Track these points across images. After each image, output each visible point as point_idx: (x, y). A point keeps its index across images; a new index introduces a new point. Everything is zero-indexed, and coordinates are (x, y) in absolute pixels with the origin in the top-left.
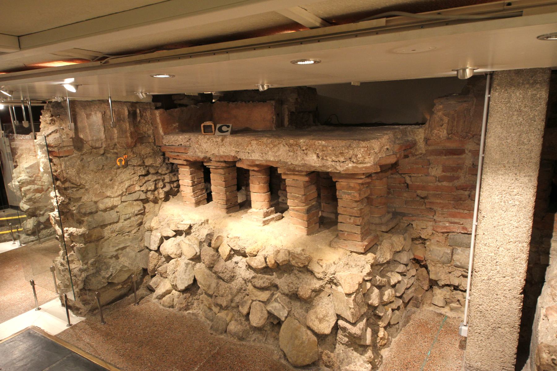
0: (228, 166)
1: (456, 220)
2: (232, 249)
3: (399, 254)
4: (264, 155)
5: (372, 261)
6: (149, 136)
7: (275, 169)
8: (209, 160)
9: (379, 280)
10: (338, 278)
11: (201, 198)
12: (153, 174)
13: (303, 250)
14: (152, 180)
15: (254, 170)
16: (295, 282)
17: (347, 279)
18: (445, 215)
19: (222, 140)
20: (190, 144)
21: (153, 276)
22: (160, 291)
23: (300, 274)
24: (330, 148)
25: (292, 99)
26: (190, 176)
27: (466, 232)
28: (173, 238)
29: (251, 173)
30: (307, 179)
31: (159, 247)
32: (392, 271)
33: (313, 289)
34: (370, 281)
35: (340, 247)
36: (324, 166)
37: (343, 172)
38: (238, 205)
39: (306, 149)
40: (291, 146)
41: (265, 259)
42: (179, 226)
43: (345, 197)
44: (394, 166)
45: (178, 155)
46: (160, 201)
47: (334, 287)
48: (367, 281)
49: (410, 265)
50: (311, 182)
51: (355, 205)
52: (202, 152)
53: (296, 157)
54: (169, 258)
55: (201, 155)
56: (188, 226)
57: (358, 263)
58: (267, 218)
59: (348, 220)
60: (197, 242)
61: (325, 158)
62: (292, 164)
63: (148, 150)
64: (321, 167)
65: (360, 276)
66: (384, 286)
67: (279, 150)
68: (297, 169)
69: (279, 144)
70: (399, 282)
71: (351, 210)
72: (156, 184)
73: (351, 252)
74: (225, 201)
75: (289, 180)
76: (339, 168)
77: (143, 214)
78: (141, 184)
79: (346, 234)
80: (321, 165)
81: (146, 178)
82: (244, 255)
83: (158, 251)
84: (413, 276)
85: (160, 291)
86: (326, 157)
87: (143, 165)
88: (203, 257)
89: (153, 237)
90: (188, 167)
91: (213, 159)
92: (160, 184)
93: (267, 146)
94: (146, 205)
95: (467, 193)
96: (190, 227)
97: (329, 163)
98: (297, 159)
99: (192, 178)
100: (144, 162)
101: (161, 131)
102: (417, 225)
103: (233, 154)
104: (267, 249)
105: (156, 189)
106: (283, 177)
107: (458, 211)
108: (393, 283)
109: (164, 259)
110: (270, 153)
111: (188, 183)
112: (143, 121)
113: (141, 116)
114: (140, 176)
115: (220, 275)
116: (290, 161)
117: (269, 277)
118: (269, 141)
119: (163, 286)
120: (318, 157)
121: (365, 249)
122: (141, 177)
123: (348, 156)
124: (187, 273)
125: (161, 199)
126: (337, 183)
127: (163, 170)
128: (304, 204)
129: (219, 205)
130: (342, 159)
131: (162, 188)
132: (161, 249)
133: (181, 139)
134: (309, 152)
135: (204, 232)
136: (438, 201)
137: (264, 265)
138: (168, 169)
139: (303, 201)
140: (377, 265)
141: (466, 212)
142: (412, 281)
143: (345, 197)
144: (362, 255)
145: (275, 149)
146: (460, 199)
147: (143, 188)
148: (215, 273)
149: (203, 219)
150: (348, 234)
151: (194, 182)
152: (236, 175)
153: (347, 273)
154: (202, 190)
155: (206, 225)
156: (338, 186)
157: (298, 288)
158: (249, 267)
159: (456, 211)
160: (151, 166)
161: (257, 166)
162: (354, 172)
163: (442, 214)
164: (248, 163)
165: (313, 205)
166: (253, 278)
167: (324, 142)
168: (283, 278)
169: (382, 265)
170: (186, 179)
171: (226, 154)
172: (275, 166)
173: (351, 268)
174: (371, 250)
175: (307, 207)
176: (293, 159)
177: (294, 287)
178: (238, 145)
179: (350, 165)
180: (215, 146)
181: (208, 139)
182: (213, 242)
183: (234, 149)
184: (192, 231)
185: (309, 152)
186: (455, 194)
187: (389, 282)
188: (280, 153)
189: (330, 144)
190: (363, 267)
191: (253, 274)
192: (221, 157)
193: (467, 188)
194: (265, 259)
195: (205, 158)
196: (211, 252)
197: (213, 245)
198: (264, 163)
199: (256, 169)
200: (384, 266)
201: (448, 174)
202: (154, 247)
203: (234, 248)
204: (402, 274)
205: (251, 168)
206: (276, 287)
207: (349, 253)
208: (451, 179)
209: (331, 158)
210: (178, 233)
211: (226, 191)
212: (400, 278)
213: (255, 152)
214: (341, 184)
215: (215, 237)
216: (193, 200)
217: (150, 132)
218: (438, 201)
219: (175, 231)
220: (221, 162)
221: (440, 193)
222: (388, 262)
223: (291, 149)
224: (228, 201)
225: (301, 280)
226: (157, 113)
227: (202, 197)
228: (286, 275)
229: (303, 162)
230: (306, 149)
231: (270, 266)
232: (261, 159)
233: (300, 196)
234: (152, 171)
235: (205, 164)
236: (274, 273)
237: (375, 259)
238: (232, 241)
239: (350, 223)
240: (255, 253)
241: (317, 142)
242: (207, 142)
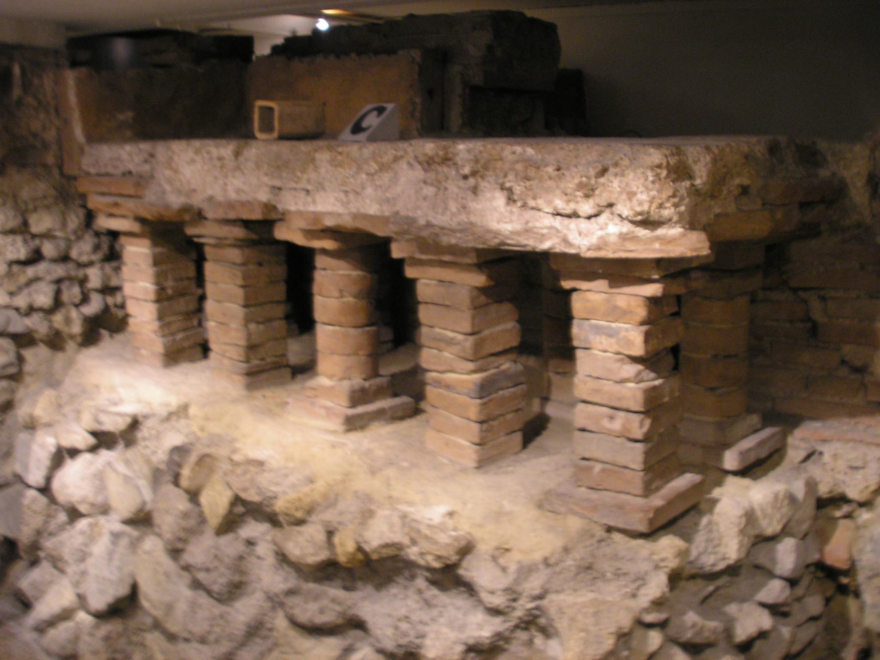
0: (254, 236)
2: (237, 500)
3: (770, 545)
4: (352, 196)
5: (673, 563)
6: (45, 146)
7: (384, 244)
8: (199, 216)
9: (694, 626)
10: (552, 611)
11: (183, 339)
12: (55, 261)
13: (451, 514)
14: (49, 278)
15: (324, 251)
16: (415, 617)
17: (580, 617)
21: (34, 563)
22: (44, 609)
25: (475, 46)
29: (320, 261)
30: (479, 280)
31: (49, 479)
32: (743, 600)
33: (471, 642)
34: (662, 625)
38: (278, 365)
39: (474, 173)
40: (428, 163)
41: (330, 534)
42: (103, 418)
44: (773, 255)
45: (116, 205)
46: (71, 346)
47: (539, 640)
48: (650, 626)
49: (805, 582)
50: (492, 294)
51: (631, 369)
52: (179, 192)
53: (445, 202)
54: (74, 514)
55: (176, 201)
56: (129, 420)
57: (626, 567)
58: (360, 410)
60: (146, 470)
61: (532, 203)
62: (429, 225)
63: (42, 187)
65: (628, 609)
66: (710, 645)
67: (395, 180)
68: (445, 240)
69: (396, 159)
70: (762, 635)
71: (618, 387)
72: (58, 293)
73: (610, 529)
74: (241, 351)
75: (427, 282)
77: (16, 377)
78: (13, 288)
81: (31, 271)
82: (273, 520)
83: (45, 490)
84: (813, 619)
85: (44, 609)
86: (534, 198)
87: (23, 229)
88: (157, 519)
89: (35, 448)
90: (146, 242)
91: (210, 214)
92: (72, 293)
93: (360, 169)
94: (28, 354)
97: (545, 221)
98: (446, 208)
100: (25, 224)
101: (78, 132)
102: (835, 456)
103: (263, 196)
104: (341, 506)
105: (58, 304)
106: (410, 272)
108: (742, 633)
109: (62, 517)
110: (369, 191)
112: (30, 100)
113: (26, 86)
114: (11, 263)
115: (201, 576)
116: (424, 214)
117: (340, 593)
119: (55, 597)
120: (511, 200)
121: (651, 521)
122: (15, 268)
124: (116, 563)
125: (72, 337)
126: (575, 297)
127: (83, 250)
128: (471, 366)
129: (226, 362)
130: (586, 208)
131: (77, 306)
132: (56, 485)
133: (128, 155)
134: (483, 184)
135: (158, 444)
137: (323, 555)
138: (97, 248)
139: (469, 353)
140: (693, 577)
142: (807, 633)
143: (599, 342)
144: (640, 542)
145: (385, 178)
147: (21, 301)
148: (187, 568)
149: (174, 401)
150: (603, 471)
152: (281, 271)
153: (586, 596)
155: (183, 422)
156: (577, 304)
157: (423, 636)
158: (283, 558)
160: (47, 235)
161: (334, 233)
162: (624, 255)
164: (303, 224)
165: (505, 375)
166: (291, 592)
167: (530, 151)
169: (712, 576)
170: (138, 279)
171: (244, 198)
172: (381, 234)
173: (600, 583)
174: (675, 527)
175: (477, 377)
176: (434, 207)
177: (412, 633)
178: (279, 166)
182: (186, 472)
184: (139, 435)
185: (483, 184)
187: (728, 633)
188: (399, 189)
189: (551, 158)
190: (641, 580)
191: (293, 581)
192: (231, 205)
194: (330, 534)
195: (186, 209)
196: (182, 504)
197: (184, 482)
198: (348, 222)
199: (329, 244)
200: (719, 582)
202: (36, 477)
203: (243, 495)
204: (776, 610)
205: (316, 244)
206: (358, 624)
207: (600, 533)
209: (549, 203)
210: (103, 440)
211: (248, 320)
212: (765, 621)
213: (336, 189)
214: (589, 298)
215: (193, 458)
216: (158, 345)
217: (50, 135)
219: (94, 434)
222: (733, 570)
223: (431, 175)
224: (252, 348)
226: (71, 77)
229: (463, 217)
230: (474, 173)
231: (342, 559)
233: (460, 337)
234: (48, 249)
237: (683, 554)
238: (239, 471)
239: (609, 433)
240: (299, 515)
242: (193, 161)
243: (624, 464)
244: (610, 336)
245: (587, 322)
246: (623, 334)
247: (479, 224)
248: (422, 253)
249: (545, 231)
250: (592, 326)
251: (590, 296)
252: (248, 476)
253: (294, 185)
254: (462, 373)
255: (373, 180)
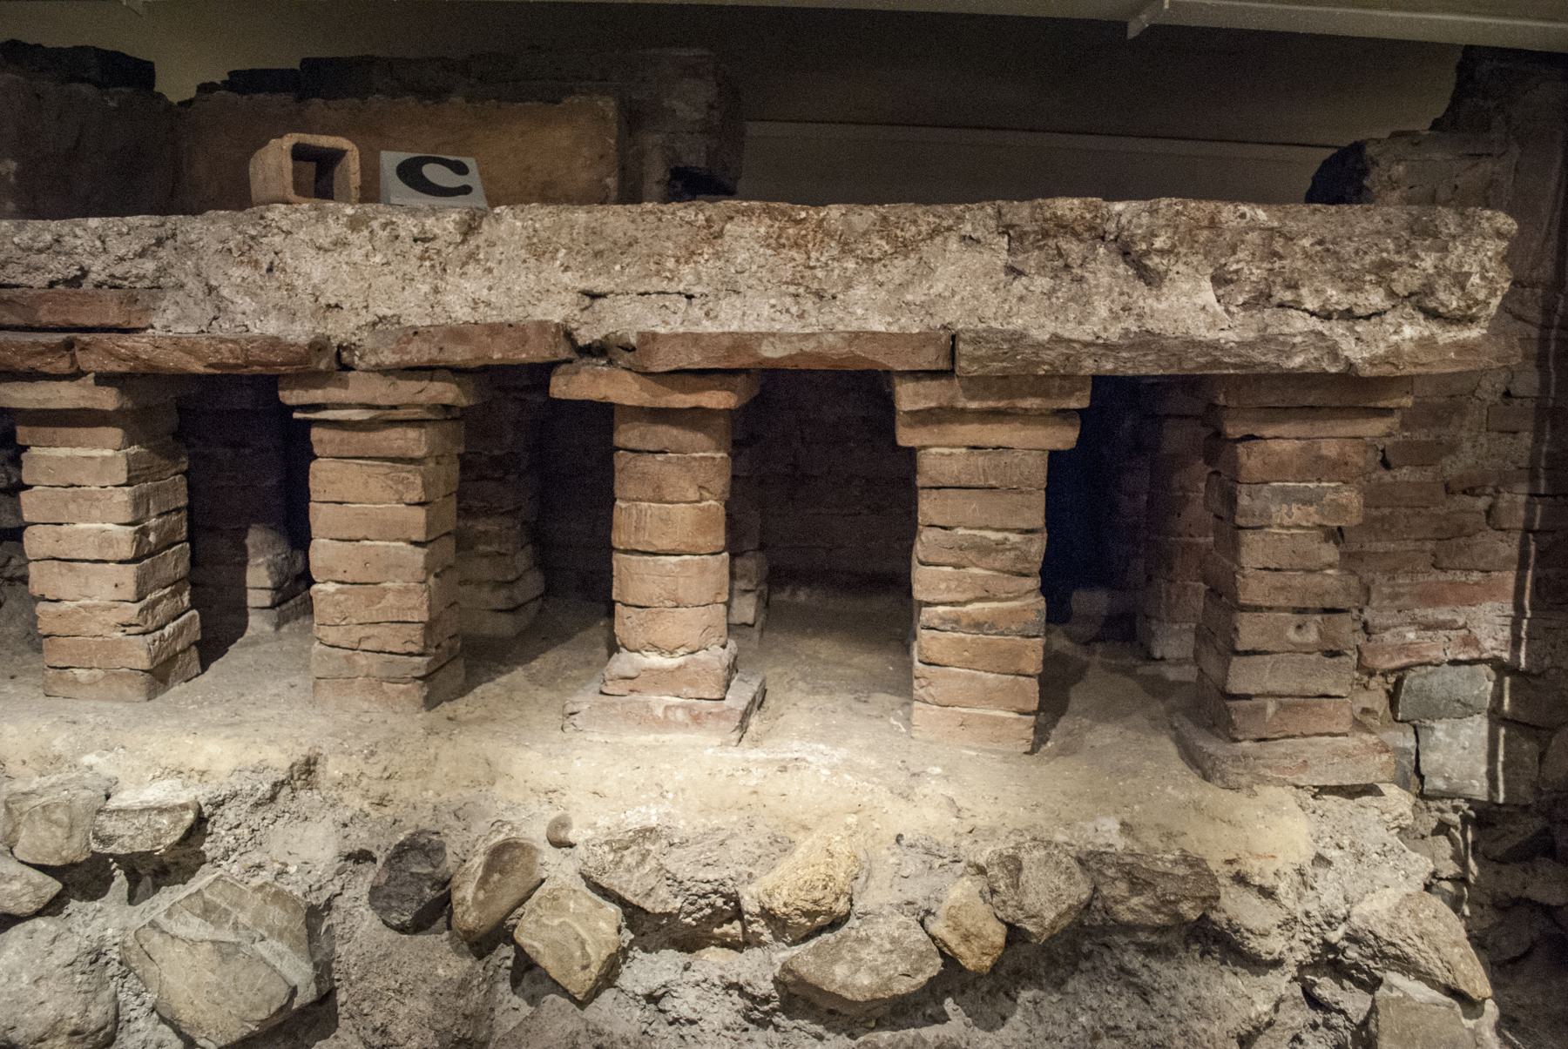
1: (1443, 614)
4: (809, 304)
18: (1405, 601)
19: (469, 229)
20: (162, 271)
23: (1155, 965)
24: (1306, 242)
26: (123, 496)
27: (1475, 655)
28: (41, 923)
35: (1264, 781)
36: (1266, 340)
37: (1368, 371)
43: (1281, 512)
59: (1292, 634)
64: (1251, 345)
69: (934, 233)
75: (941, 454)
76: (1350, 349)
79: (1271, 706)
80: (1251, 335)
86: (1293, 286)
95: (1482, 503)
96: (199, 828)
99: (139, 502)
103: (555, 311)
107: (1449, 576)
111: (106, 540)
118: (864, 217)
123: (1404, 282)
136: (1380, 547)
141: (1476, 576)
143: (1281, 512)
146: (1461, 531)
149: (279, 760)
151: (144, 532)
154: (177, 584)
159: (1442, 577)
163: (1395, 596)
167: (1261, 215)
168: (1017, 1018)
171: (493, 317)
179: (1408, 331)
180: (411, 266)
181: (355, 224)
183: (567, 278)
186: (1441, 511)
192: (459, 334)
193: (1484, 486)
201: (1421, 435)
208: (1425, 455)
218: (1380, 547)
220: (427, 371)
221: (1387, 511)
225: (1160, 1002)
227: (179, 632)
228: (1025, 995)
232: (795, 328)
235: (290, 397)
236: (949, 1005)
238: (630, 858)
241: (1228, 213)
242: (341, 243)
243: (1321, 690)
244: (1307, 502)
245: (1266, 487)
246: (1329, 497)
247: (1169, 334)
248: (973, 398)
249: (1298, 339)
250: (1274, 491)
251: (1275, 445)
252: (651, 864)
253: (664, 285)
254: (1007, 599)
255: (870, 271)
